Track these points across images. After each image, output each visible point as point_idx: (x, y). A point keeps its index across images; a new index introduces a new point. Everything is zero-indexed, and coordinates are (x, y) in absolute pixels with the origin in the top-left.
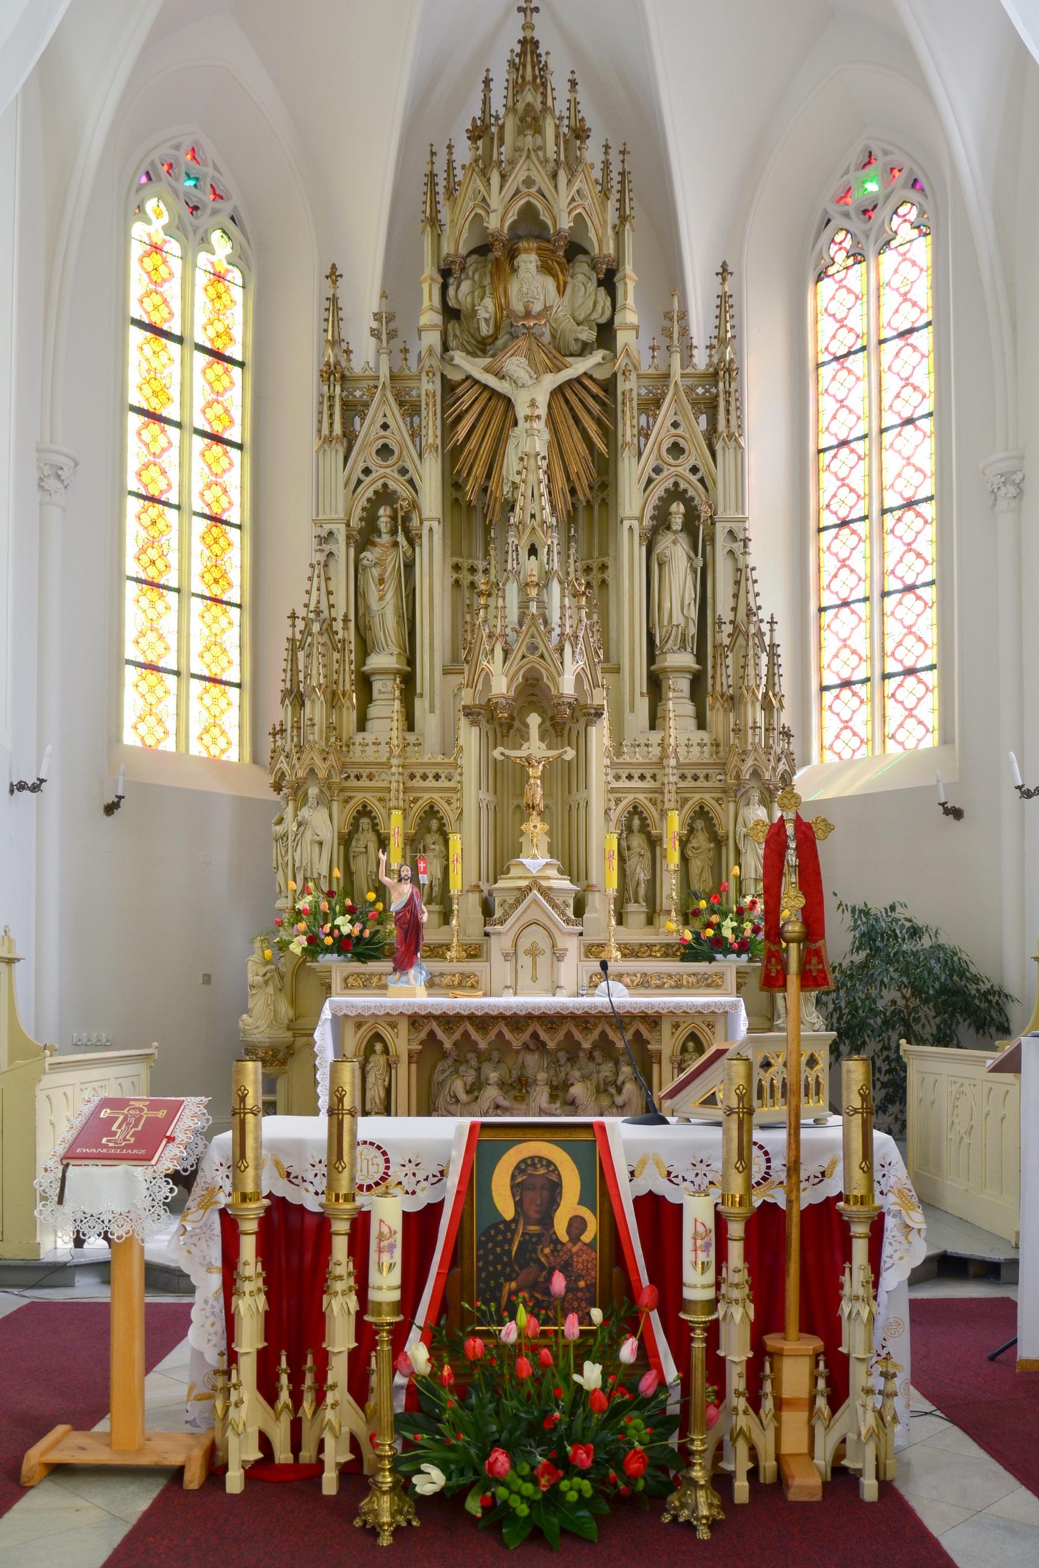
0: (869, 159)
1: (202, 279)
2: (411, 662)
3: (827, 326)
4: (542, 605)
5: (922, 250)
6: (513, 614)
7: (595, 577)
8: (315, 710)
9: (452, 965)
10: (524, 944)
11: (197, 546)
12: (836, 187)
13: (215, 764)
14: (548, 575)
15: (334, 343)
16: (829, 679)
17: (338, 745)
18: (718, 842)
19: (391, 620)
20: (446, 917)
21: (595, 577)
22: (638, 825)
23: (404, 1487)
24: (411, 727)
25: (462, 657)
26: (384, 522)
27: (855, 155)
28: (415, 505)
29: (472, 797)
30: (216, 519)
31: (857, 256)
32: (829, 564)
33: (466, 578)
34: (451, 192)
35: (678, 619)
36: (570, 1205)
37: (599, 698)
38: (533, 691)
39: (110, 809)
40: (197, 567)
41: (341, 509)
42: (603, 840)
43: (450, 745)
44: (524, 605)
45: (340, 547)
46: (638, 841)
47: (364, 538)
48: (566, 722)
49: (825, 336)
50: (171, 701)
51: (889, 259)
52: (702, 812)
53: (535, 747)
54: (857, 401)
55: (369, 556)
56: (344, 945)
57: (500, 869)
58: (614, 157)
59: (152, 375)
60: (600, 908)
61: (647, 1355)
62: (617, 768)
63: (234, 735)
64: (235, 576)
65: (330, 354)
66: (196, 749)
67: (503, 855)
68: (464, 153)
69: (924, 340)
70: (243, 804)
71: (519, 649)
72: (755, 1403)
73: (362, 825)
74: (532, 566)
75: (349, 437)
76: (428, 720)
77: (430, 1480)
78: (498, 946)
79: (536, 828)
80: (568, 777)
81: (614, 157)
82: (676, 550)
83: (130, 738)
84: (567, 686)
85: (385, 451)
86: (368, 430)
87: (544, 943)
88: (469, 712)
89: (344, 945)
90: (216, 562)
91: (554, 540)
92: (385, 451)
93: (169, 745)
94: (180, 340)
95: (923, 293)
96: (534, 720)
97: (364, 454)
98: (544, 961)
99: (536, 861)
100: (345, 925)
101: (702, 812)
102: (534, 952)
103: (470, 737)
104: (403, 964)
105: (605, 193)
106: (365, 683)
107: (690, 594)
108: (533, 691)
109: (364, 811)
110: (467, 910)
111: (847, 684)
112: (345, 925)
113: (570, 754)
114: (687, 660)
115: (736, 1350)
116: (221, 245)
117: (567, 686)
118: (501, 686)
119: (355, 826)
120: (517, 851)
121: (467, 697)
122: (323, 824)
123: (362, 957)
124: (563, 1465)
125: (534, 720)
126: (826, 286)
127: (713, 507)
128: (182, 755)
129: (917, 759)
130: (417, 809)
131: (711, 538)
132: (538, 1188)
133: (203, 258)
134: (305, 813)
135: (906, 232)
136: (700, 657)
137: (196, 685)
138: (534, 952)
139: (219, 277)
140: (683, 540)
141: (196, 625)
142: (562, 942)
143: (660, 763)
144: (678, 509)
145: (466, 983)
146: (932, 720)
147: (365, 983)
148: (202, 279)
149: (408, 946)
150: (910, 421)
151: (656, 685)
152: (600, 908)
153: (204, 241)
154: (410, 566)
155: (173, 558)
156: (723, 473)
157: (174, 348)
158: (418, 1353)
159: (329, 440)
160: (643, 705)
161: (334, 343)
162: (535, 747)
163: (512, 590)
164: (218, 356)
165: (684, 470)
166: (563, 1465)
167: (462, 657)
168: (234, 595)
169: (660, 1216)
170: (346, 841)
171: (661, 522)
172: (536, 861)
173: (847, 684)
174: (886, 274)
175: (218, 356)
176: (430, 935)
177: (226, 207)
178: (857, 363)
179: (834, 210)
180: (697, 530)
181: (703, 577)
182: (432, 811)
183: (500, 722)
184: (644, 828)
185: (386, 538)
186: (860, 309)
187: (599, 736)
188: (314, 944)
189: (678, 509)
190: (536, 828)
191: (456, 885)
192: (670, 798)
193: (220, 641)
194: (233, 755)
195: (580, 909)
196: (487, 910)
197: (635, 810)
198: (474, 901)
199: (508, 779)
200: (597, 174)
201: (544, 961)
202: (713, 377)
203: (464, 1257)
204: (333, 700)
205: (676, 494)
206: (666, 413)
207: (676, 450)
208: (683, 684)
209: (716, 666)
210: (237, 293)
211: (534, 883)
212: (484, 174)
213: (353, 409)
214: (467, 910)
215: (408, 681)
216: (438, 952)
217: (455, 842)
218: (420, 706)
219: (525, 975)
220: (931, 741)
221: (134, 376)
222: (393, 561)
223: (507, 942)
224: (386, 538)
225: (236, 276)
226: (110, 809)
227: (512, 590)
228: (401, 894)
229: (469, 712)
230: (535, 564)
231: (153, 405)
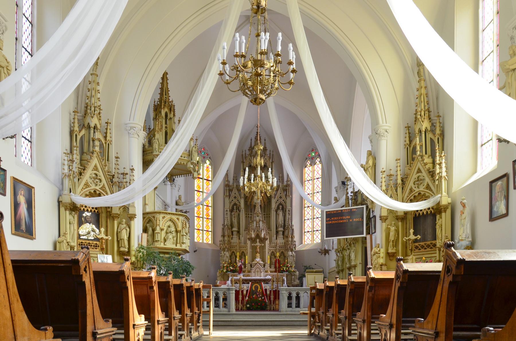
0: (313, 150)
1: (205, 168)
2: (239, 229)
3: (306, 175)
4: (259, 224)
5: (320, 166)
6: (255, 226)
7: (268, 216)
8: (226, 238)
9: (246, 273)
10: (256, 271)
11: (205, 210)
12: (308, 154)
13: (207, 244)
14: (260, 220)
15: (227, 181)
16: (306, 231)
17: (229, 242)
18: (285, 257)
19: (236, 223)
20: (245, 267)
21: (268, 216)
22: (273, 254)
23: (246, 305)
24: (239, 239)
25: (247, 229)
26: (235, 208)
27: (311, 149)
28: (240, 206)
29: (249, 250)
30: (207, 206)
31: (311, 165)
32: (306, 213)
33: (248, 216)
34: (246, 157)
35: (280, 223)
36: (259, 289)
37: (268, 237)
38: (258, 236)
39: (195, 251)
40: (205, 213)
41: (228, 207)
42: (268, 257)
43: (245, 243)
44: (256, 224)
45: (229, 213)
46: (273, 256)
47: (232, 211)
48: (263, 240)
49: (306, 177)
50: (201, 235)
51: (316, 166)
52: (282, 252)
53: (258, 244)
54: (311, 187)
55: (233, 213)
56: (232, 271)
57: (253, 260)
58: (271, 152)
59: (198, 185)
60: (267, 266)
61: (264, 299)
62: (270, 246)
63: (210, 239)
64: (210, 214)
65: (226, 183)
66: (205, 242)
67: (253, 258)
68: (248, 153)
69: (320, 180)
70: (213, 250)
71: (256, 231)
72: (274, 304)
73: (233, 255)
74: (258, 218)
75: (230, 195)
76: (242, 239)
77: (248, 306)
78: (252, 271)
79: (258, 255)
80: (263, 248)
81: (271, 152)
82: (281, 213)
83: (196, 241)
84: (263, 236)
85: (235, 197)
86: (233, 194)
87: (259, 270)
88: (249, 239)
89: (232, 271)
90: (208, 213)
91: (261, 215)
92: (235, 197)
93: (201, 241)
94: (202, 179)
95: (320, 172)
96: (258, 240)
97: (232, 198)
98: (259, 273)
99: (258, 259)
100: (231, 268)
101: (282, 252)
102: (258, 272)
103: (249, 242)
104: (240, 273)
105: (270, 158)
106: (232, 232)
107: (282, 219)
108: (258, 236)
109: (233, 252)
110: (248, 266)
111: (308, 232)
112: (231, 268)
113: (263, 245)
114: (282, 229)
115: (272, 299)
116: (208, 162)
117: (263, 236)
118: (253, 236)
119: (232, 254)
120: (255, 258)
121: (248, 237)
122: (228, 254)
123: (234, 272)
124: (258, 305)
125: (258, 240)
126: (306, 169)
127: (286, 206)
128: (203, 243)
129: (317, 243)
130: (241, 252)
131: (286, 211)
132: (256, 288)
133: (205, 165)
134: (225, 253)
135: (318, 163)
136: (284, 229)
137: (205, 232)
138: (258, 272)
139: (208, 167)
140: (282, 211)
141: (205, 223)
142: (262, 270)
143: (276, 246)
144: (281, 206)
145: (248, 276)
146: (320, 238)
147: (234, 276)
148: (205, 168)
149: (240, 271)
150: (318, 192)
151: (277, 232)
152: (267, 266)
153: (206, 163)
154: (239, 215)
155: (201, 212)
156: (288, 201)
157: (201, 180)
158: (247, 298)
159: (227, 196)
160: (275, 236)
161: (227, 181)
162: (258, 244)
163: (255, 223)
164: (208, 180)
165: (282, 201)
166: (258, 305)
167: (247, 229)
168: (210, 218)
169: (266, 290)
170: (230, 256)
171: (278, 208)
172: (258, 259)
173: (308, 232)
174: (315, 169)
175: (208, 180)
176: (243, 270)
177: (209, 156)
178: (311, 182)
179: (307, 157)
180: (284, 209)
181: (285, 217)
182: (243, 252)
183: (253, 240)
184: (274, 255)
185: (235, 210)
186: (311, 174)
187: (267, 242)
188: (227, 271)
189: (281, 206)
190: (258, 255)
191: (247, 262)
192: (278, 251)
193: (208, 225)
194: (210, 242)
195: (264, 266)
196: (251, 266)
197: (273, 252)
198: (249, 265)
199: (254, 248)
200: (269, 155)
201: (259, 273)
202: (286, 186)
203: (251, 292)
204: (229, 236)
205: (280, 204)
206: (279, 192)
207: (281, 197)
208: (281, 233)
209: (285, 230)
210: (210, 169)
211: (258, 262)
212: (251, 156)
213: (231, 191)
214: (248, 266)
215: (238, 232)
216: (244, 272)
217: (247, 257)
218: (241, 236)
219: (256, 275)
220: (320, 241)
221: (196, 185)
222: (236, 214)
223: (254, 270)
224: (235, 210)
225: (210, 167)
226: (195, 251)
227: (255, 223)
228: (239, 264)
229: (249, 239)
230: (258, 216)
231: (198, 189)
